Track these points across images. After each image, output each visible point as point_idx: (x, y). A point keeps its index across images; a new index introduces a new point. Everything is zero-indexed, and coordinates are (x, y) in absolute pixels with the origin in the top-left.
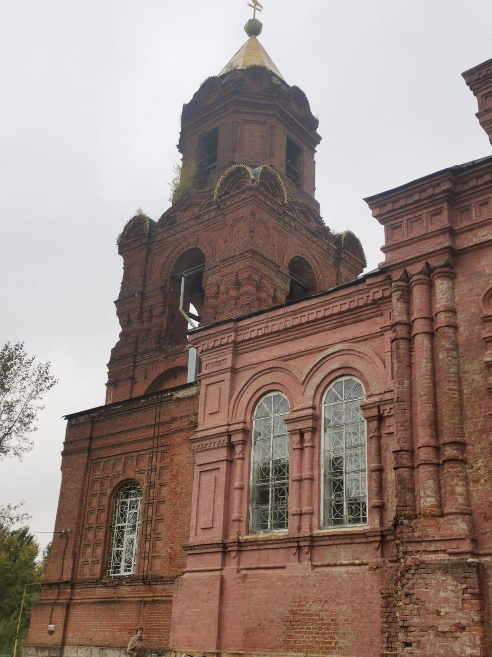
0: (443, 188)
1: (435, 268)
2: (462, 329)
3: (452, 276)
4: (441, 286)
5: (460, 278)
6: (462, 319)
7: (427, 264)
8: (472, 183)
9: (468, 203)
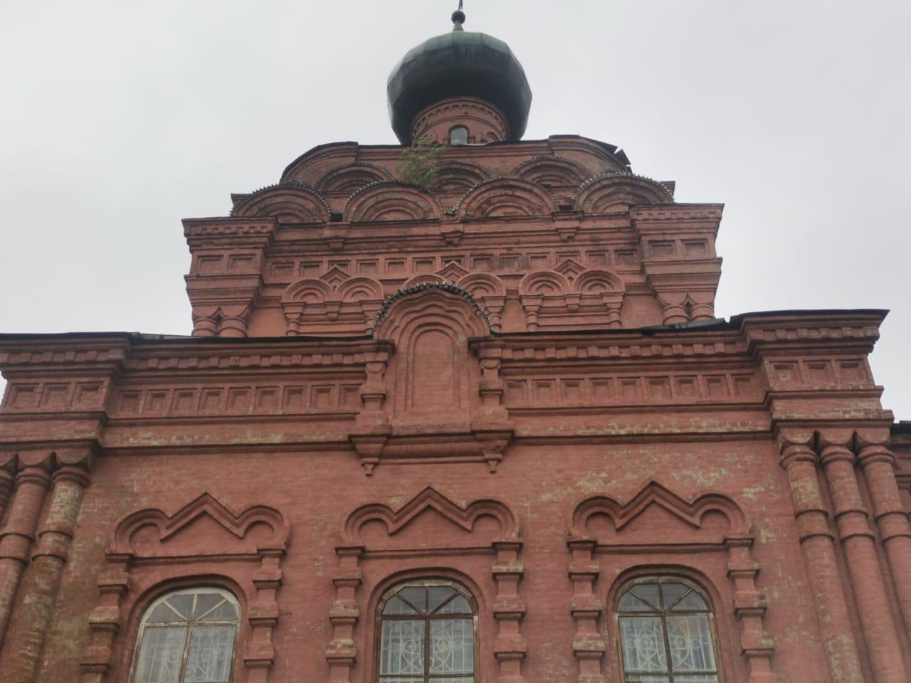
0: (111, 357)
1: (64, 465)
2: (72, 565)
3: (83, 483)
4: (64, 493)
5: (94, 489)
6: (78, 550)
7: (53, 456)
8: (152, 363)
9: (138, 388)
